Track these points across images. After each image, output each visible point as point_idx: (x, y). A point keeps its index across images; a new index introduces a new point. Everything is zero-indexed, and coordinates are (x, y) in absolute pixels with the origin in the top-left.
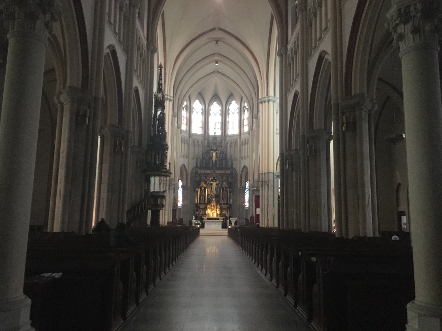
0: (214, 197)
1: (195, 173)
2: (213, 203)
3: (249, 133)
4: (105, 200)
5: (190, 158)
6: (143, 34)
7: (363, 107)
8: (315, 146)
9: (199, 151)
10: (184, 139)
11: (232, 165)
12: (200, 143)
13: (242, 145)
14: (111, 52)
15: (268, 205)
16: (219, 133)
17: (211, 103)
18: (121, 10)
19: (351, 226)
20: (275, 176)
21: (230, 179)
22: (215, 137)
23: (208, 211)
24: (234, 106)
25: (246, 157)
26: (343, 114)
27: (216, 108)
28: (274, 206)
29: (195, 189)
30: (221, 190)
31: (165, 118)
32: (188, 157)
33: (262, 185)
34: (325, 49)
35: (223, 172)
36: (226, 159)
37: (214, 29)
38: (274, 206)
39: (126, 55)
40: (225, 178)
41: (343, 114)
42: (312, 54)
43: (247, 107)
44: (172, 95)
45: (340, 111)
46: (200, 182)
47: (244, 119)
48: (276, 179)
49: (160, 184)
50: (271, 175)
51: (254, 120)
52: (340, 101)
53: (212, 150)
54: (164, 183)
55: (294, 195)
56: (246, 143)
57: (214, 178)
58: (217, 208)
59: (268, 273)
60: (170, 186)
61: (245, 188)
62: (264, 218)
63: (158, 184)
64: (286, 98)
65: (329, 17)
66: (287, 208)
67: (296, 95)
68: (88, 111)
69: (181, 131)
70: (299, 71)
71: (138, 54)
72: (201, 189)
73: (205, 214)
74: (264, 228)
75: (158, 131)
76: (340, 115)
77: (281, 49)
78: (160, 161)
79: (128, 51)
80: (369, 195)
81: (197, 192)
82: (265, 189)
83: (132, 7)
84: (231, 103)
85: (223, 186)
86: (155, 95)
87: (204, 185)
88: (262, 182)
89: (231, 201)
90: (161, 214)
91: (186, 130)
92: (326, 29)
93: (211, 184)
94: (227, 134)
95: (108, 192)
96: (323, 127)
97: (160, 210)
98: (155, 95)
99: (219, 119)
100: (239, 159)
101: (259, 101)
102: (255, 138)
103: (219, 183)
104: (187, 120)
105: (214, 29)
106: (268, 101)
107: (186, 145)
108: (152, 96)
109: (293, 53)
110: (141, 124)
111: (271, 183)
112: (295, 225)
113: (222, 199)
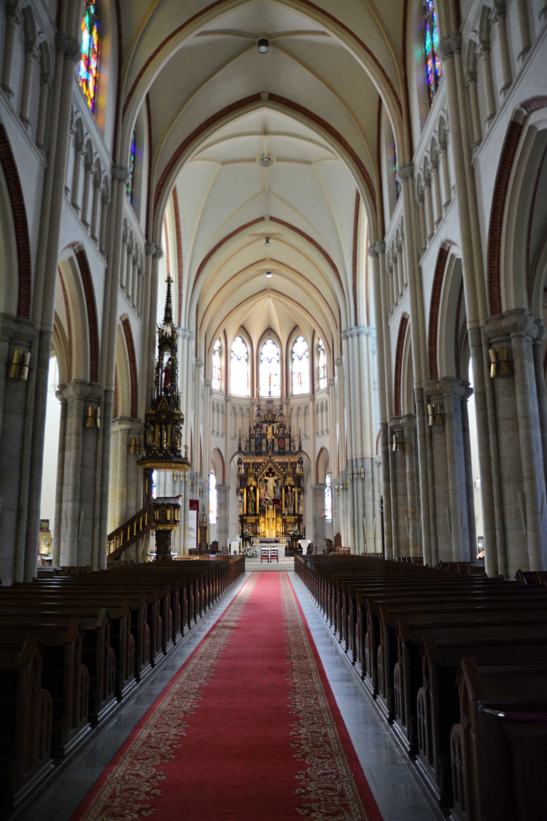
0: (272, 502)
1: (238, 463)
2: (271, 514)
3: (328, 391)
4: (69, 514)
5: (229, 437)
6: (138, 229)
7: (524, 333)
8: (442, 407)
9: (243, 425)
10: (218, 404)
11: (300, 448)
12: (245, 408)
14: (77, 255)
16: (276, 393)
18: (96, 185)
19: (513, 551)
20: (375, 464)
21: (298, 470)
23: (262, 528)
24: (301, 347)
25: (325, 432)
26: (490, 346)
27: (270, 350)
28: (374, 516)
30: (283, 491)
31: (176, 368)
32: (225, 434)
35: (286, 460)
36: (289, 436)
37: (262, 219)
38: (374, 516)
39: (105, 262)
40: (289, 470)
41: (490, 346)
43: (323, 347)
45: (483, 341)
46: (247, 478)
47: (319, 368)
48: (376, 469)
49: (174, 482)
52: (481, 323)
55: (409, 496)
56: (324, 408)
57: (270, 469)
59: (358, 659)
61: (324, 485)
63: (172, 483)
64: (388, 327)
65: (453, 181)
66: (397, 520)
67: (404, 321)
68: (28, 356)
70: (407, 279)
73: (256, 534)
74: (358, 557)
75: (166, 390)
76: (484, 347)
77: (375, 245)
78: (169, 444)
79: (109, 253)
80: (543, 493)
83: (116, 183)
85: (287, 483)
86: (159, 329)
87: (254, 484)
90: (172, 537)
92: (448, 203)
93: (266, 481)
95: (74, 500)
98: (159, 329)
99: (276, 368)
100: (312, 437)
101: (343, 334)
102: (338, 399)
103: (279, 479)
104: (221, 372)
105: (262, 219)
107: (220, 414)
109: (396, 250)
110: (136, 380)
112: (411, 550)
113: (286, 506)
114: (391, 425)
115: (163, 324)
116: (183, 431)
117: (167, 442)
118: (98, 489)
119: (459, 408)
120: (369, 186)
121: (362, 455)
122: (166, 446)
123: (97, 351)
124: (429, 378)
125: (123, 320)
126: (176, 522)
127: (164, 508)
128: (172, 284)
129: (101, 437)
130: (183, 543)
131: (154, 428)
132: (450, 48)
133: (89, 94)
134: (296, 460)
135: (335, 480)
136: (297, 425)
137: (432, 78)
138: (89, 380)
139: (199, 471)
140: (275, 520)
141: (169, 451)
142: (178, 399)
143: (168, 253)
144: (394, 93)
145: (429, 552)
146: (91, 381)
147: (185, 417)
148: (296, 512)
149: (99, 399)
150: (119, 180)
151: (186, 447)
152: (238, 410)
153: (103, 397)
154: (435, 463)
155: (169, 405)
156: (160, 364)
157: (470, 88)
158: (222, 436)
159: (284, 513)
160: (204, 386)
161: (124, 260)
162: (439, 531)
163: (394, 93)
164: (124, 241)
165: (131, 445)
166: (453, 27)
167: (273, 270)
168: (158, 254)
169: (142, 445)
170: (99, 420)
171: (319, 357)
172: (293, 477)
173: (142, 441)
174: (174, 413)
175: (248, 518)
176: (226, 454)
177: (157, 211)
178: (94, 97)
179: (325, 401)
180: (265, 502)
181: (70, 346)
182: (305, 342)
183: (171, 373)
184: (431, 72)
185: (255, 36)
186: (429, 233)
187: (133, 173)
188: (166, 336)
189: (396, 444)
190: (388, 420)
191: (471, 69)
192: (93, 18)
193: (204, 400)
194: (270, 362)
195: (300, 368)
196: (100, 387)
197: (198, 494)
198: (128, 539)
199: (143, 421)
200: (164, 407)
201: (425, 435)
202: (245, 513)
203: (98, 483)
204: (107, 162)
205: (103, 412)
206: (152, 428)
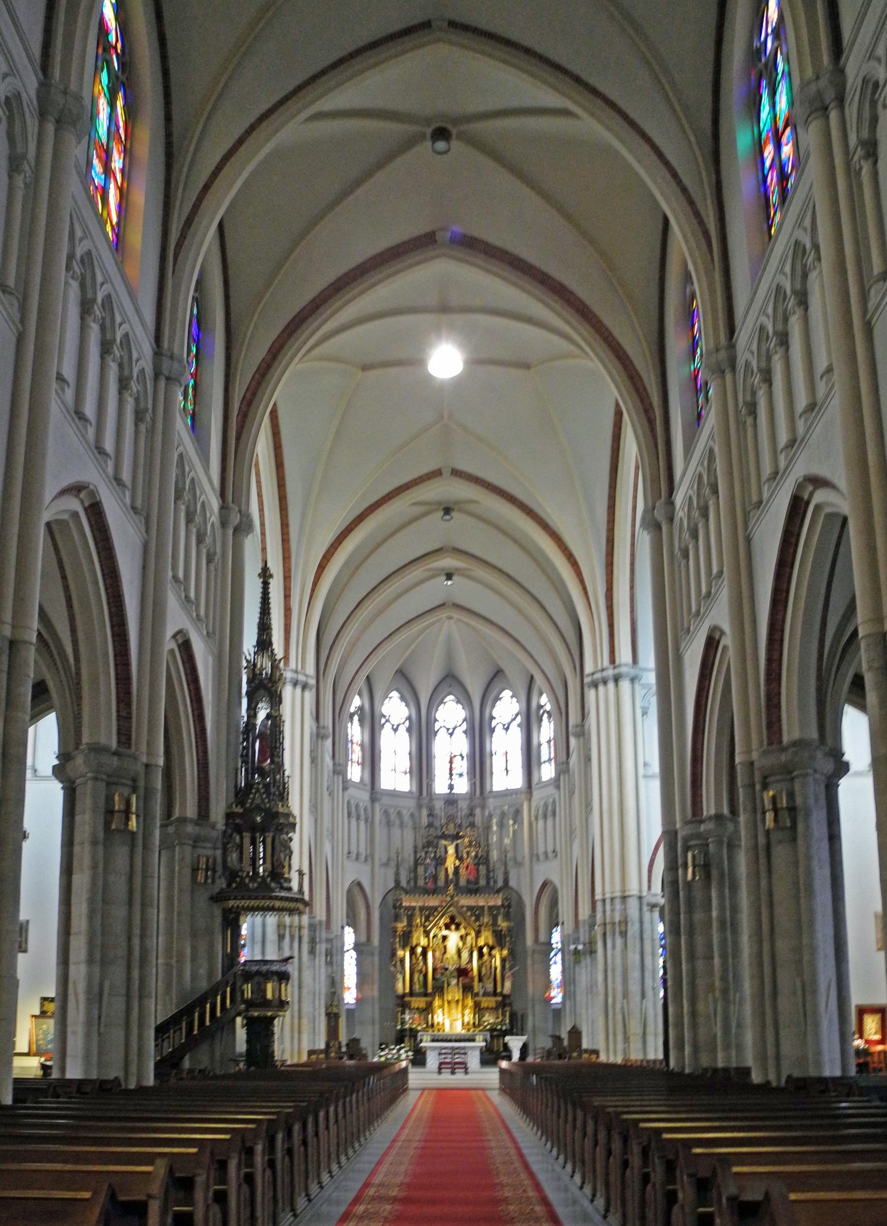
0: (455, 974)
1: (395, 907)
2: (454, 993)
3: (556, 782)
6: (208, 479)
8: (791, 795)
9: (406, 841)
10: (357, 806)
11: (506, 881)
13: (536, 818)
15: (625, 995)
17: (435, 700)
20: (645, 908)
22: (451, 800)
24: (507, 707)
25: (550, 855)
29: (394, 954)
31: (281, 732)
32: (370, 858)
33: (605, 934)
34: (817, 470)
35: (481, 903)
37: (436, 474)
40: (486, 919)
42: (765, 496)
43: (548, 707)
44: (311, 669)
47: (540, 745)
49: (281, 937)
50: (633, 904)
51: (573, 741)
53: (444, 837)
54: (292, 938)
55: (717, 961)
56: (549, 813)
57: (452, 919)
58: (464, 1007)
60: (313, 941)
62: (615, 1035)
64: (679, 659)
66: (693, 1001)
69: (346, 784)
71: (188, 531)
72: (413, 952)
78: (269, 865)
81: (402, 961)
82: (614, 947)
83: (162, 383)
84: (497, 698)
87: (423, 941)
88: (605, 924)
89: (508, 984)
90: (276, 1030)
91: (362, 778)
92: (721, 573)
94: (488, 789)
96: (814, 734)
97: (272, 1018)
99: (461, 744)
101: (587, 680)
105: (436, 474)
106: (617, 679)
107: (362, 823)
108: (239, 663)
110: (205, 752)
111: (633, 929)
113: (480, 980)
114: (684, 833)
115: (255, 653)
116: (295, 845)
117: (264, 863)
118: (136, 942)
119: (823, 797)
120: (642, 400)
121: (624, 891)
122: (264, 871)
123: (128, 692)
124: (765, 743)
125: (180, 642)
126: (282, 1004)
127: (261, 979)
128: (271, 581)
129: (139, 848)
130: (296, 1040)
131: (242, 838)
132: (822, 100)
133: (109, 214)
134: (499, 903)
135: (569, 936)
136: (498, 842)
137: (772, 179)
138: (114, 744)
139: (324, 918)
140: (460, 1003)
141: (269, 879)
142: (284, 788)
143: (262, 525)
144: (697, 214)
145: (762, 1058)
146: (119, 746)
147: (298, 820)
148: (499, 990)
149: (134, 780)
150: (168, 379)
151: (301, 874)
152: (393, 817)
153: (142, 776)
154: (776, 898)
155: (268, 797)
156: (250, 725)
157: (748, 423)
158: (366, 860)
159: (476, 991)
160: (331, 774)
161: (174, 518)
162: (783, 1019)
163: (697, 214)
164: (178, 497)
165: (198, 869)
166: (826, 59)
167: (457, 569)
168: (243, 528)
169: (219, 869)
170: (134, 817)
171: (540, 726)
172: (494, 932)
173: (219, 860)
174: (277, 813)
175: (414, 999)
176: (372, 884)
177: (242, 445)
178: (118, 223)
179: (551, 800)
180: (442, 974)
181: (79, 683)
182: (515, 699)
183: (272, 740)
184: (771, 167)
185: (428, 121)
186: (767, 469)
187: (195, 376)
188: (261, 674)
189: (694, 867)
190: (678, 826)
191: (865, 134)
192: (117, 77)
193: (333, 798)
194: (451, 734)
195: (506, 745)
196: (135, 758)
197: (323, 958)
198: (195, 1032)
199: (221, 826)
200: (258, 801)
201: (756, 846)
202: (407, 990)
203: (137, 931)
204: (144, 346)
205: (141, 804)
206: (238, 838)
